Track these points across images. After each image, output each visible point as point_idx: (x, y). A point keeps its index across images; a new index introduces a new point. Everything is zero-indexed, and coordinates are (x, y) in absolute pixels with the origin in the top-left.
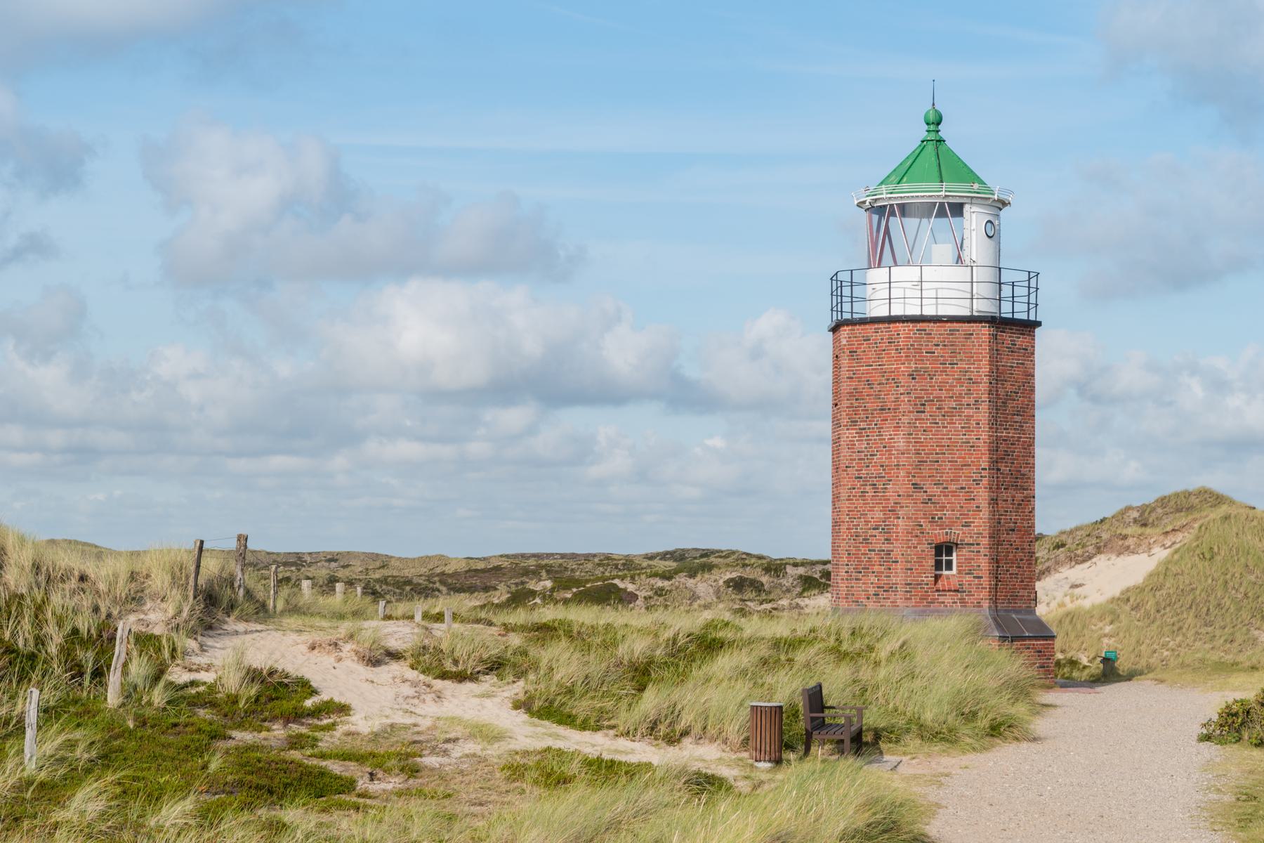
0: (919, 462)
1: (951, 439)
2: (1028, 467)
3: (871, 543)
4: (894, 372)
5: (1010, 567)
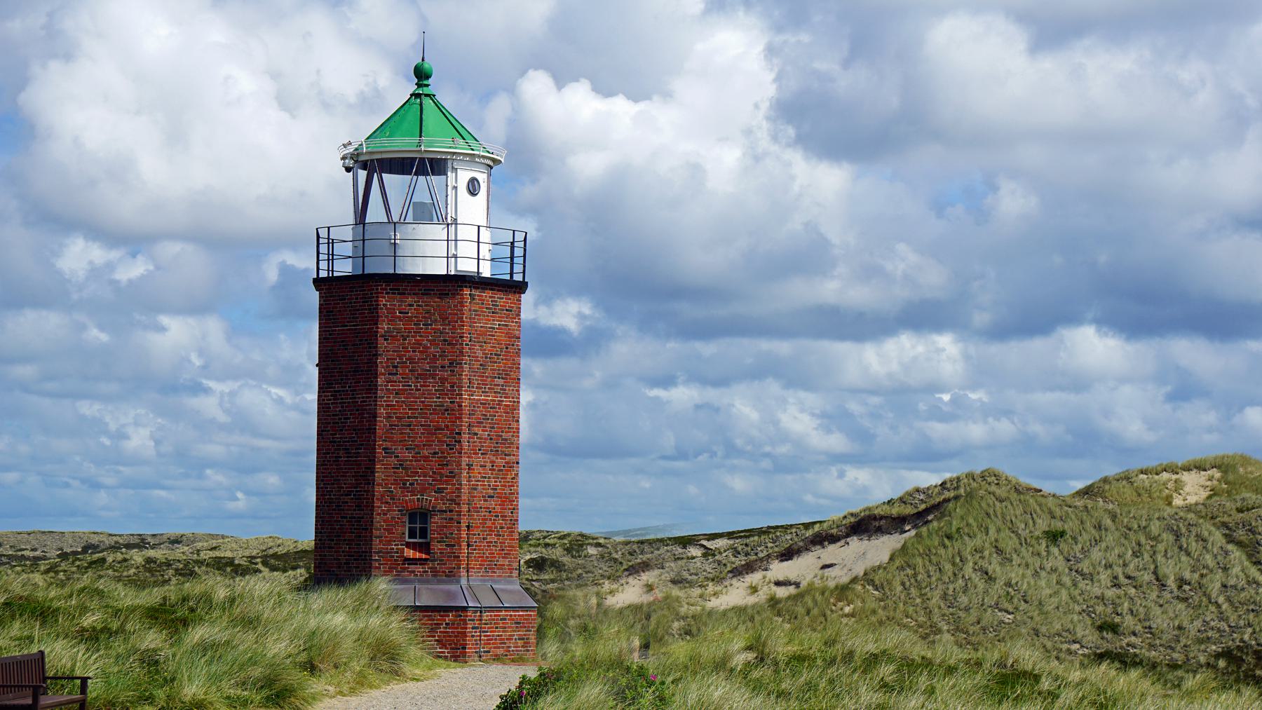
1: (423, 402)
2: (510, 432)
3: (343, 510)
4: (367, 332)
5: (487, 535)
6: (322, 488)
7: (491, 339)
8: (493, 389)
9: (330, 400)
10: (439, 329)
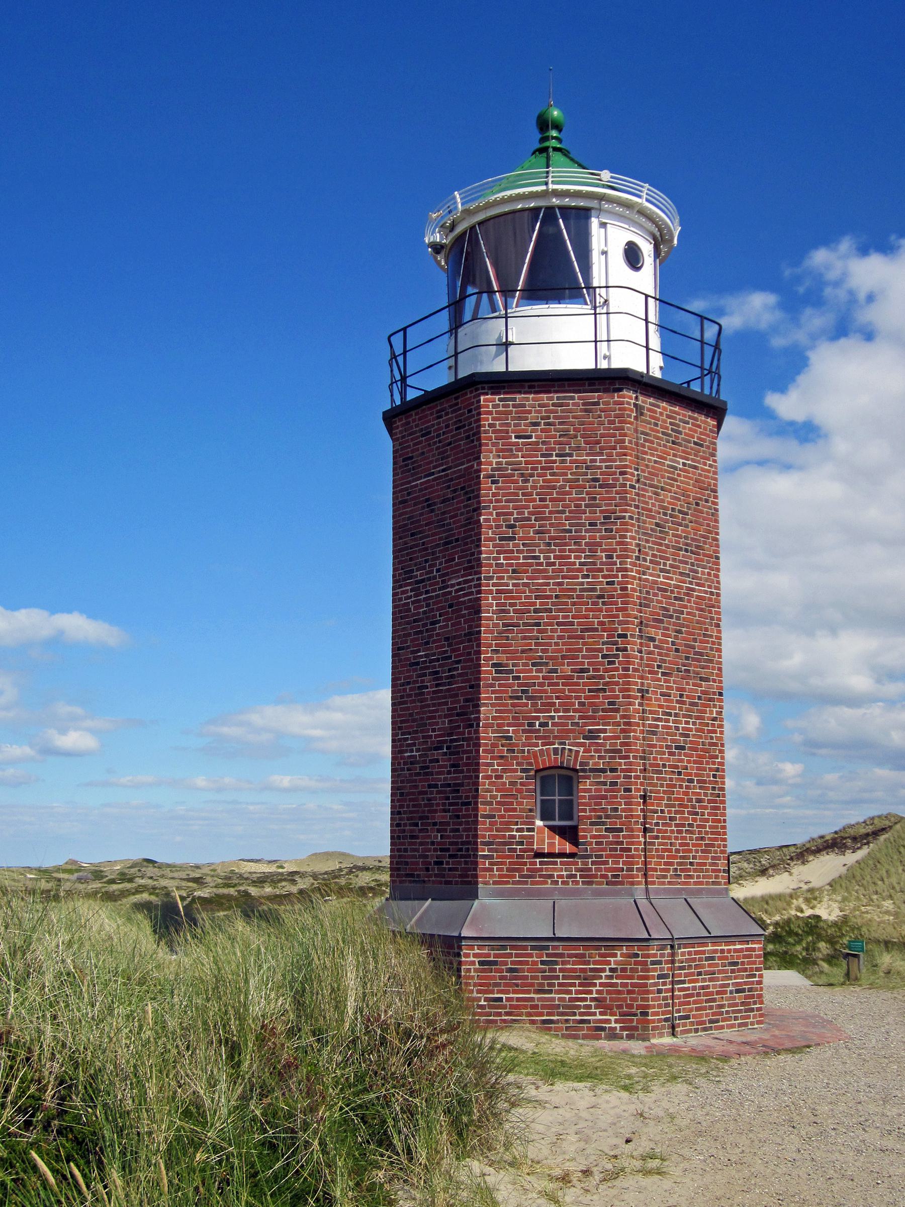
0: (504, 625)
2: (708, 642)
5: (676, 812)
6: (400, 740)
7: (672, 486)
8: (678, 568)
9: (410, 597)
10: (585, 462)
